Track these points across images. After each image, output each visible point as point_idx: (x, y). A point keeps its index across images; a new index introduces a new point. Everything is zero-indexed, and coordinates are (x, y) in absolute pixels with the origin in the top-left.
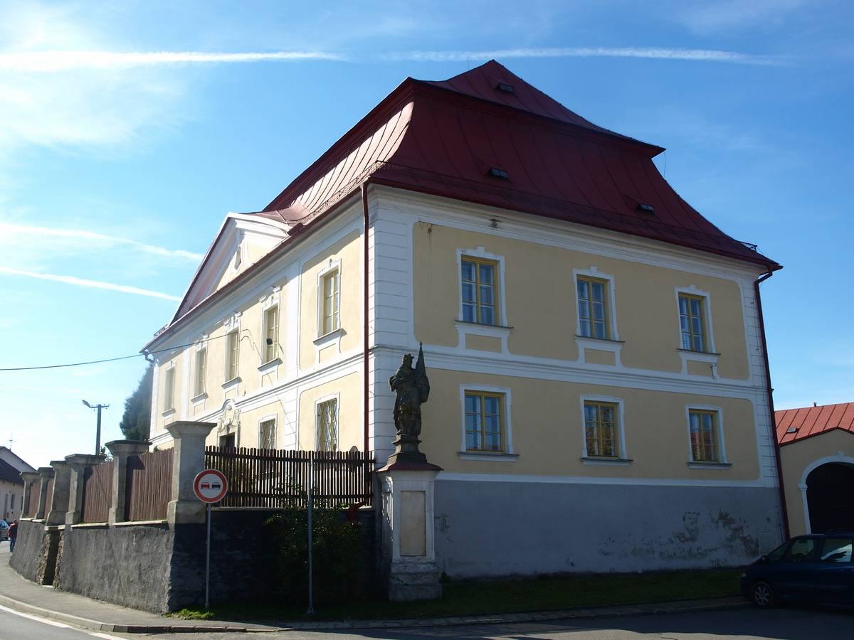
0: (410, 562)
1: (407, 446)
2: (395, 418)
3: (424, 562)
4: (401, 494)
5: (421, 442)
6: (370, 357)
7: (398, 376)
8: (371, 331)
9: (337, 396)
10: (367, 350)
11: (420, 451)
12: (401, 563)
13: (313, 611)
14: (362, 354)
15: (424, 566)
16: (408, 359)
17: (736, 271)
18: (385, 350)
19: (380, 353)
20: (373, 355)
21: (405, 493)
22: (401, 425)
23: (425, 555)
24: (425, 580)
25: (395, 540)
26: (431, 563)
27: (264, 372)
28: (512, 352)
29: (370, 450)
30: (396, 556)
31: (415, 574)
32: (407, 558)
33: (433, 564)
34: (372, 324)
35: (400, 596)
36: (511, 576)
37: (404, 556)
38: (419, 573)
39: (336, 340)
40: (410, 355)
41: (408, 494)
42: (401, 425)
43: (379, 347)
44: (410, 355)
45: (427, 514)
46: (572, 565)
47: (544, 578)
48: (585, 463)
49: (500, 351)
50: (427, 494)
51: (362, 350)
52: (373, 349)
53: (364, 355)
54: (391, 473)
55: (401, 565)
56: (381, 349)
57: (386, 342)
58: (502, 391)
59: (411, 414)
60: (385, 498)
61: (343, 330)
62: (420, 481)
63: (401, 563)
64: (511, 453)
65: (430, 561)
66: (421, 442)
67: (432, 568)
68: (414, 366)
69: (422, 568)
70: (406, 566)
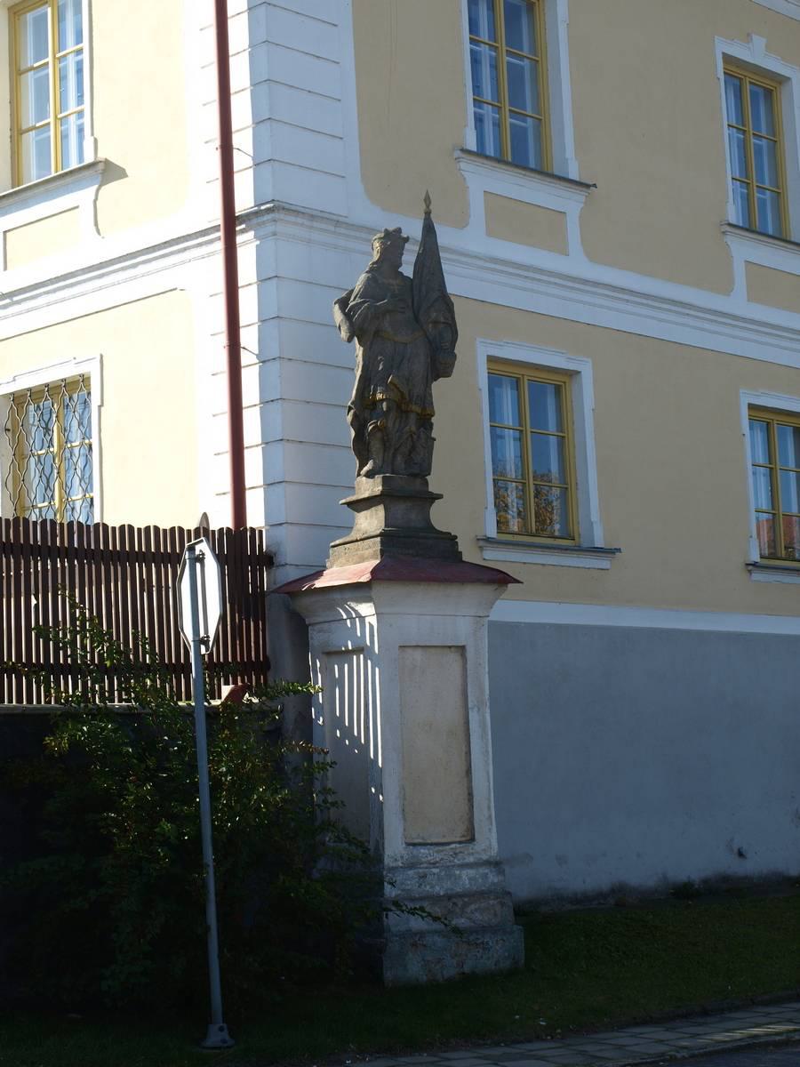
0: (434, 864)
1: (400, 508)
2: (359, 424)
3: (471, 859)
4: (401, 656)
5: (440, 497)
6: (239, 239)
7: (365, 294)
8: (241, 161)
9: (92, 370)
10: (231, 221)
11: (438, 527)
12: (412, 866)
13: (225, 1035)
14: (216, 228)
15: (471, 872)
16: (394, 241)
17: (557, 186)
18: (292, 218)
19: (280, 228)
20: (251, 234)
21: (410, 651)
22: (376, 445)
23: (472, 839)
24: (478, 916)
25: (390, 798)
26: (488, 863)
27: (463, 156)
28: (592, 255)
29: (250, 524)
30: (394, 847)
31: (449, 897)
32: (423, 851)
33: (496, 864)
34: (243, 140)
35: (414, 968)
36: (613, 891)
37: (414, 845)
38: (461, 896)
39: (84, 196)
40: (399, 231)
41: (418, 654)
42: (376, 445)
43: (271, 211)
44: (399, 231)
45: (474, 717)
46: (741, 854)
47: (684, 893)
48: (758, 576)
49: (564, 251)
50: (470, 654)
51: (217, 217)
52: (247, 217)
53: (221, 234)
54: (377, 590)
55: (411, 873)
56: (280, 215)
57: (300, 192)
58: (571, 366)
59: (407, 412)
60: (327, 671)
61: (107, 162)
62: (446, 614)
63: (412, 866)
64: (598, 544)
65: (485, 857)
66: (440, 497)
67: (493, 878)
68: (407, 270)
69: (466, 879)
70: (424, 876)
